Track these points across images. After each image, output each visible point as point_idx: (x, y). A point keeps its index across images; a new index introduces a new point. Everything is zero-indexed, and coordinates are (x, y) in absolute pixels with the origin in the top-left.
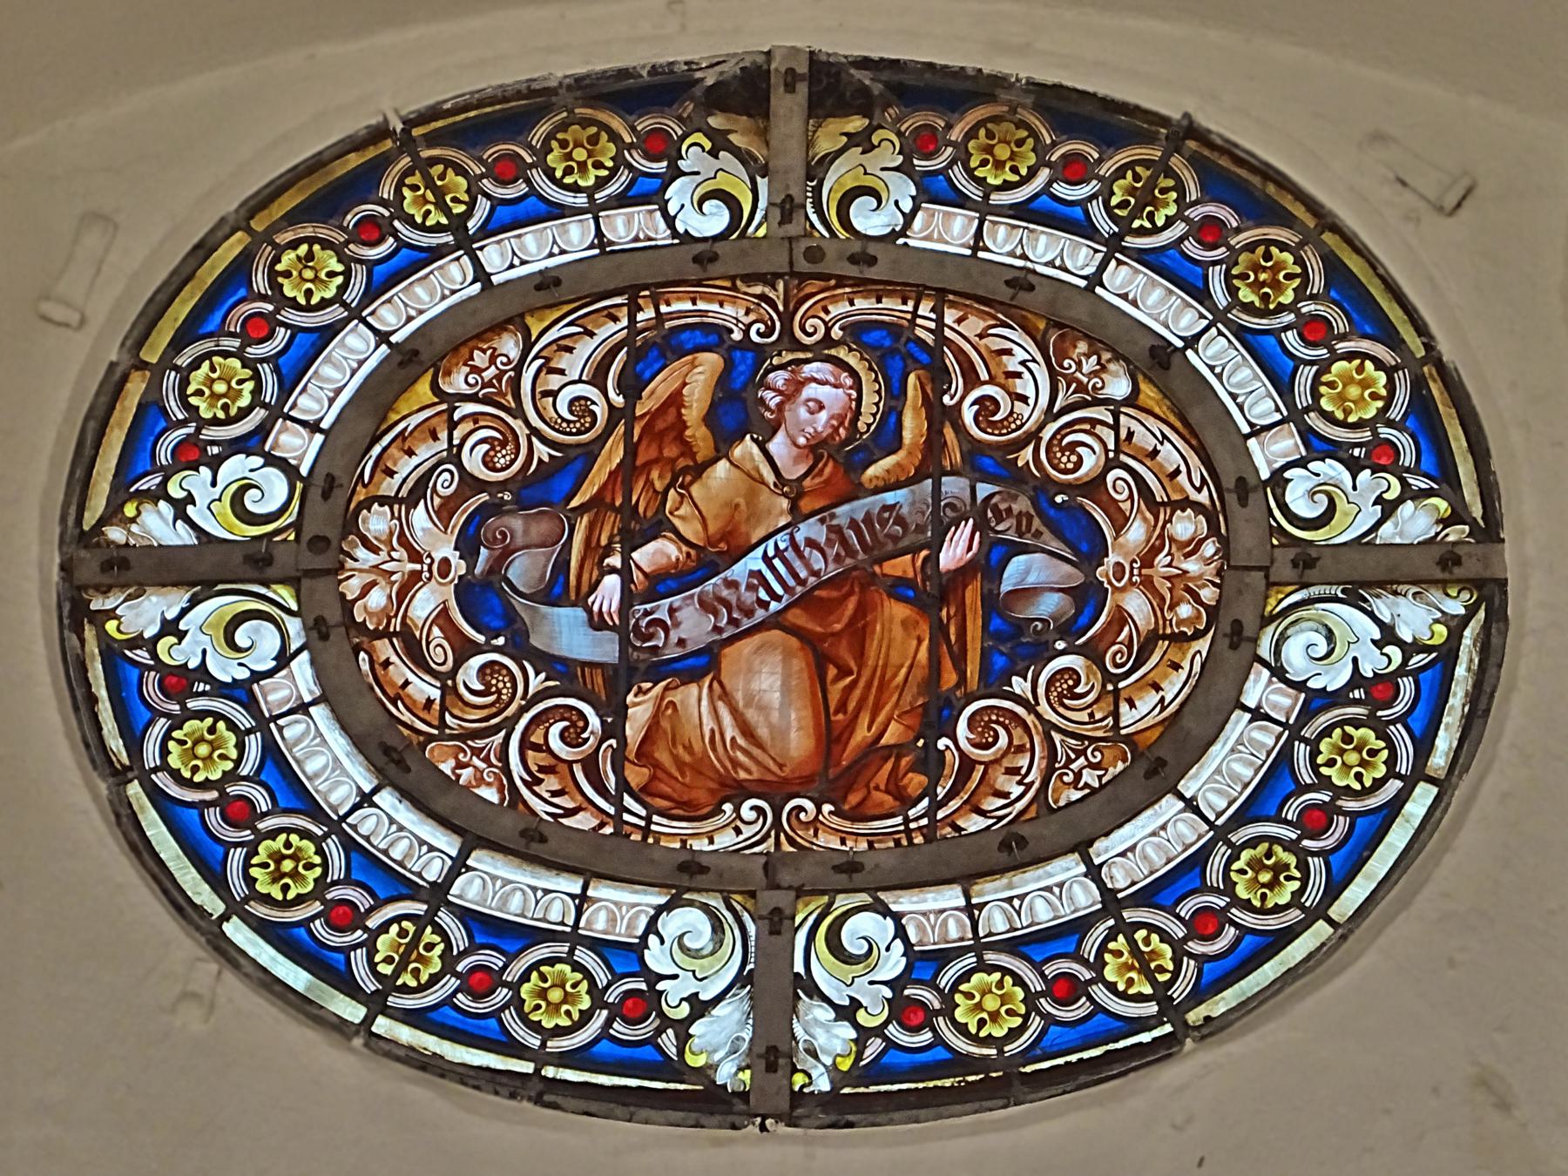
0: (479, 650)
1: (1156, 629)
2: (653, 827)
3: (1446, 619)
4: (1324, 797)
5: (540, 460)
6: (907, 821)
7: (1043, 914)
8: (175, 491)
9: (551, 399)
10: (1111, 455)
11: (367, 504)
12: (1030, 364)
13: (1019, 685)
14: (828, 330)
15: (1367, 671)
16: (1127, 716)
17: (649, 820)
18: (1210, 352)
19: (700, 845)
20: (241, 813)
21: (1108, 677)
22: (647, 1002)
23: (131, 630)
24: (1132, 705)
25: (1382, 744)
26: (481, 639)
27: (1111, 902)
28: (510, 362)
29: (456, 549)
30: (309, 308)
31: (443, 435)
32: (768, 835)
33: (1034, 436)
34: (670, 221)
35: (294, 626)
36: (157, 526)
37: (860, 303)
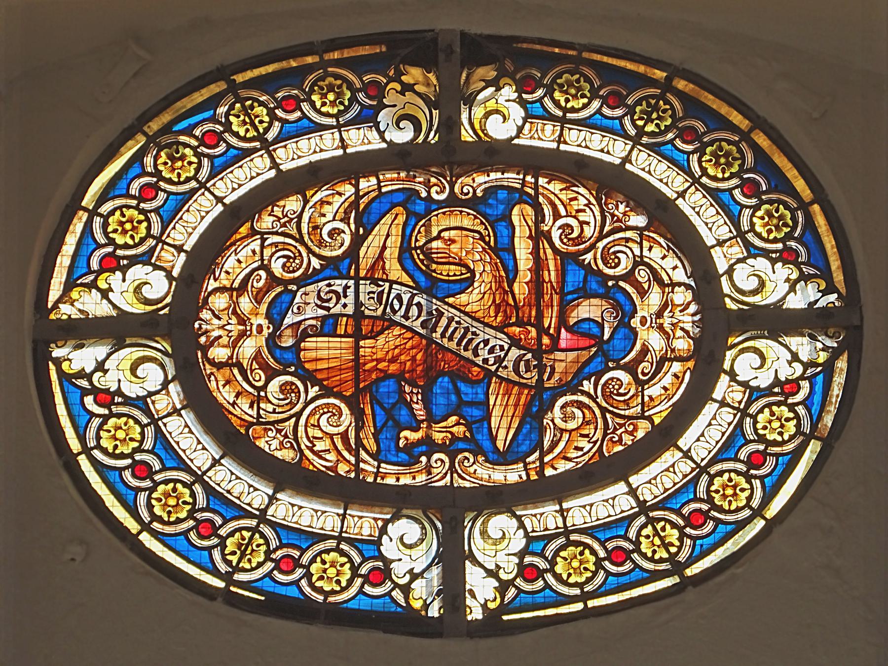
0: (623, 278)
2: (381, 470)
3: (825, 349)
4: (761, 447)
5: (314, 268)
7: (602, 513)
8: (102, 284)
13: (587, 386)
15: (118, 274)
18: (692, 200)
20: (142, 470)
22: (382, 574)
23: (76, 367)
24: (254, 252)
25: (111, 235)
26: (621, 284)
27: (643, 507)
28: (295, 213)
30: (179, 183)
31: (646, 399)
32: (446, 474)
33: (593, 246)
34: (521, 525)
35: (726, 288)
36: (802, 346)
37: (493, 175)
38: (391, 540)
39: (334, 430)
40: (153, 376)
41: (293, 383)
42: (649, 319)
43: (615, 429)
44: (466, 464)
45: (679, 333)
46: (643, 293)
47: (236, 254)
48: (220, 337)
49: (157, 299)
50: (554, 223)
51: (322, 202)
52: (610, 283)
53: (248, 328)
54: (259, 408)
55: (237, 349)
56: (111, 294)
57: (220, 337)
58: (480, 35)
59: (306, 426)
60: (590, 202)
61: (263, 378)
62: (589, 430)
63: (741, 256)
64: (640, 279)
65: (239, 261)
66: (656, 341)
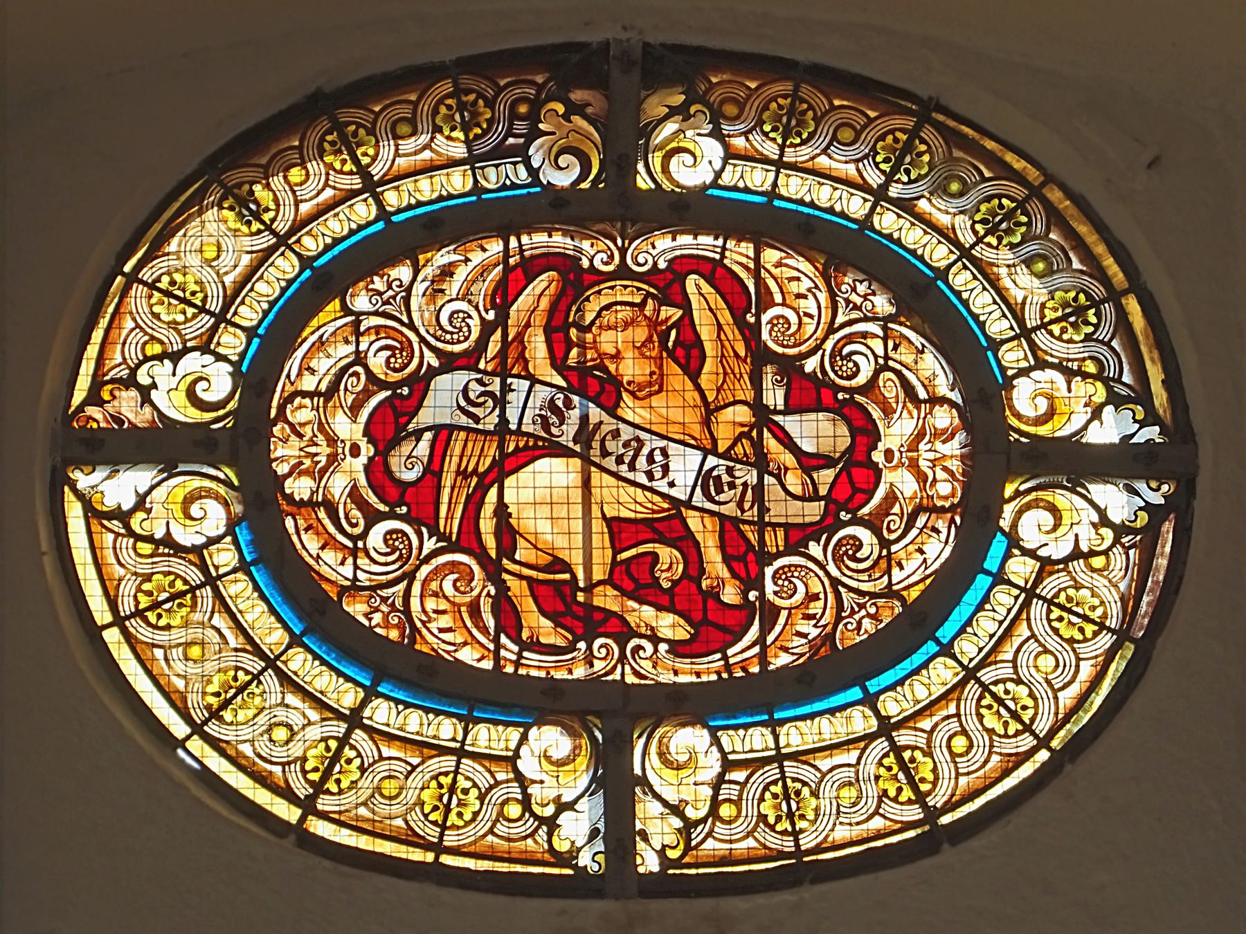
0: (862, 390)
1: (326, 402)
5: (429, 364)
10: (881, 361)
11: (290, 399)
12: (424, 618)
13: (815, 549)
16: (897, 575)
17: (520, 656)
19: (560, 675)
21: (885, 543)
24: (902, 568)
26: (382, 507)
29: (364, 436)
32: (614, 668)
36: (1115, 500)
38: (710, 162)
40: (214, 518)
41: (404, 534)
42: (897, 455)
45: (941, 475)
46: (888, 411)
49: (219, 402)
51: (447, 272)
53: (340, 450)
54: (356, 567)
56: (154, 394)
58: (663, 45)
59: (422, 596)
60: (817, 287)
61: (362, 522)
62: (816, 608)
63: (1024, 364)
64: (887, 395)
65: (921, 552)
66: (906, 484)
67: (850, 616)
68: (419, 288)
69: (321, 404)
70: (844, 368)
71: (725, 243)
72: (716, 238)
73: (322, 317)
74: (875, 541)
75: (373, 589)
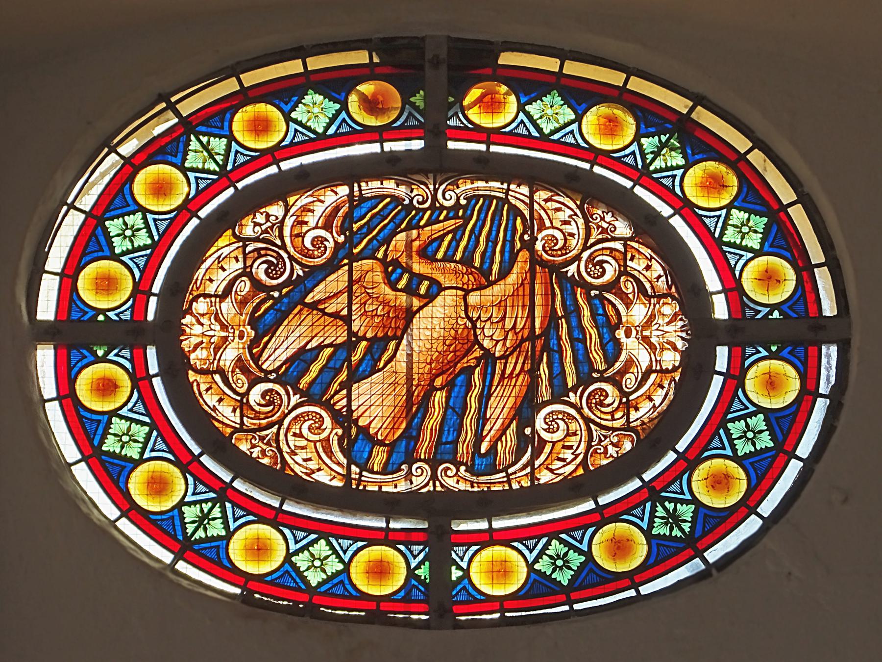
1: (220, 302)
2: (363, 478)
6: (508, 475)
9: (300, 239)
11: (195, 299)
14: (458, 198)
16: (634, 415)
21: (623, 393)
33: (578, 258)
39: (316, 438)
43: (600, 441)
44: (421, 199)
46: (628, 304)
47: (654, 405)
48: (668, 324)
50: (329, 436)
51: (306, 209)
52: (593, 293)
55: (649, 313)
57: (668, 324)
60: (576, 214)
62: (573, 441)
67: (274, 225)
68: (289, 222)
69: (654, 363)
70: (596, 272)
71: (509, 186)
72: (502, 184)
73: (221, 242)
74: (617, 393)
75: (254, 431)
